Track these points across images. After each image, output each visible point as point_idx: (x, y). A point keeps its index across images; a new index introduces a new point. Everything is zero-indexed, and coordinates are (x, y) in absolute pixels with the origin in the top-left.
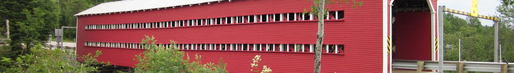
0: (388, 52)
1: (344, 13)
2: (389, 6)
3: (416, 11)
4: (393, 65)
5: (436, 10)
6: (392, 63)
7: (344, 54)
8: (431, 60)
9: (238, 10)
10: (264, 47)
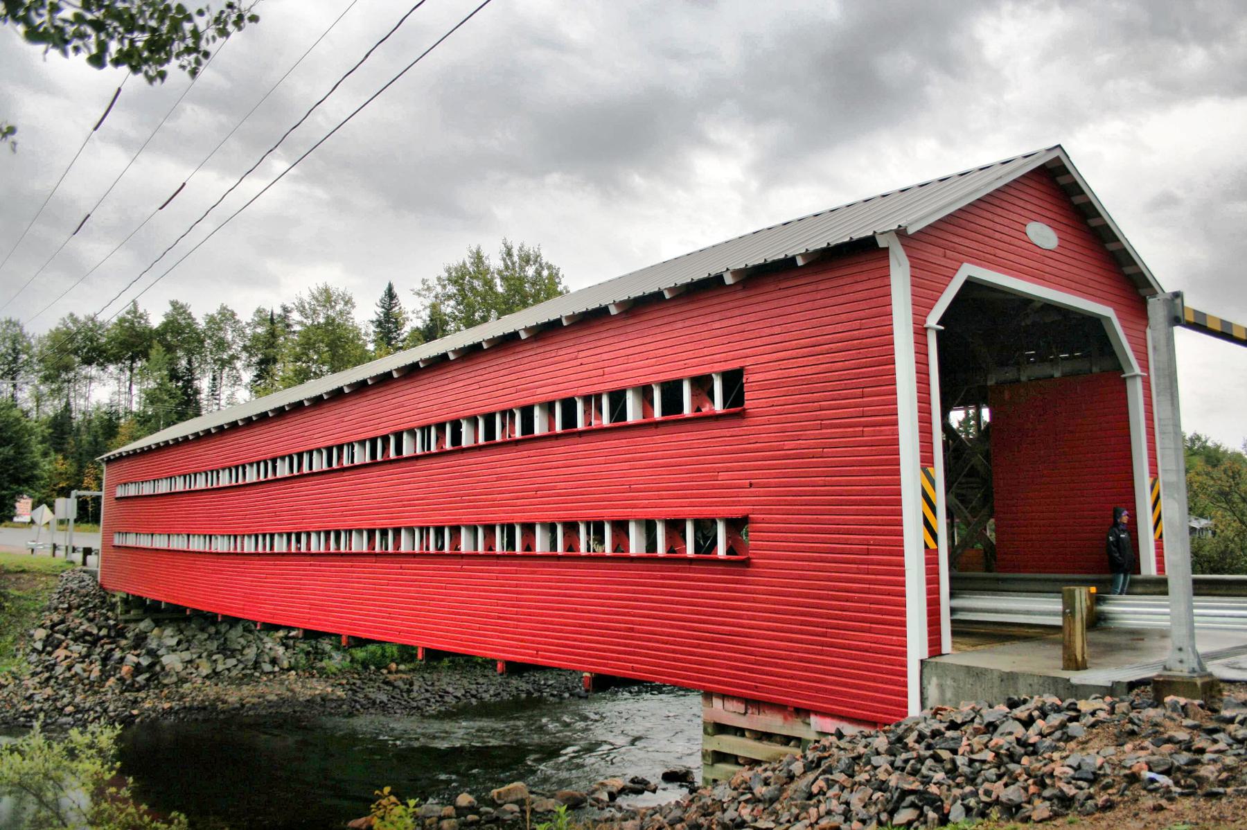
0: (926, 546)
1: (744, 381)
2: (920, 332)
3: (1064, 375)
4: (958, 603)
5: (1145, 366)
6: (952, 595)
7: (749, 559)
8: (1139, 573)
9: (421, 405)
10: (397, 537)
